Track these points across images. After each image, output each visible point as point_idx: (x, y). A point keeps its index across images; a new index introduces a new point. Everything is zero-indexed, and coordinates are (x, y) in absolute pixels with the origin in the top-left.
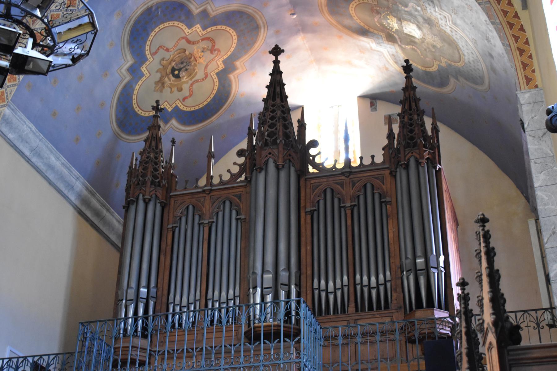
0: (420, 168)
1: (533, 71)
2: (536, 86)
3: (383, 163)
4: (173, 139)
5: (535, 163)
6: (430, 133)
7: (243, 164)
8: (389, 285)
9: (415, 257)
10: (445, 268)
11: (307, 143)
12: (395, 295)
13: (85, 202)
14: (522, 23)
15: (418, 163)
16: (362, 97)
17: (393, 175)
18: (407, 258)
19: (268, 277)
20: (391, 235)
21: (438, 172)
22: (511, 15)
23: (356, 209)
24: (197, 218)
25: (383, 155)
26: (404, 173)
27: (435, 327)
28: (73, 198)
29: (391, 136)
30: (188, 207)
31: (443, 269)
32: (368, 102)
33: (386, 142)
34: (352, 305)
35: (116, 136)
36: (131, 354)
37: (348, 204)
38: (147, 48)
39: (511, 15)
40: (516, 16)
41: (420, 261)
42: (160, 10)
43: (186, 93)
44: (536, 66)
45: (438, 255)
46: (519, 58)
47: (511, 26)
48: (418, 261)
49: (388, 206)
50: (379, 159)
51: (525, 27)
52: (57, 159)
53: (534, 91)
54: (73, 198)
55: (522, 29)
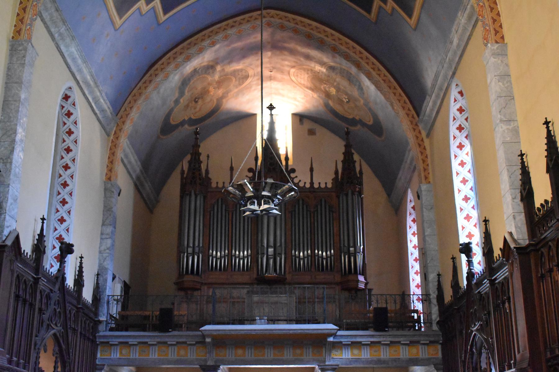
0: (354, 197)
1: (429, 173)
2: (429, 182)
3: (332, 188)
4: (208, 155)
5: (426, 223)
6: (358, 176)
7: (252, 177)
8: (333, 258)
9: (349, 247)
10: (363, 252)
11: (289, 169)
12: (336, 264)
13: (138, 178)
14: (425, 145)
15: (353, 194)
16: (294, 115)
17: (338, 197)
18: (344, 246)
19: (271, 250)
20: (335, 231)
21: (362, 199)
22: (422, 147)
23: (316, 213)
24: (224, 206)
25: (332, 183)
26: (345, 198)
27: (358, 285)
28: (134, 177)
29: (336, 172)
30: (218, 200)
31: (362, 253)
32: (298, 119)
33: (334, 176)
34: (313, 267)
35: (158, 137)
36: (234, 302)
37: (312, 210)
38: (187, 89)
39: (420, 139)
40: (422, 140)
41: (352, 249)
42: (200, 70)
43: (198, 109)
44: (430, 171)
45: (361, 245)
46: (423, 165)
47: (420, 145)
48: (351, 249)
49: (334, 214)
50: (330, 186)
51: (426, 148)
52: (134, 157)
53: (428, 185)
54: (134, 177)
55: (425, 148)
